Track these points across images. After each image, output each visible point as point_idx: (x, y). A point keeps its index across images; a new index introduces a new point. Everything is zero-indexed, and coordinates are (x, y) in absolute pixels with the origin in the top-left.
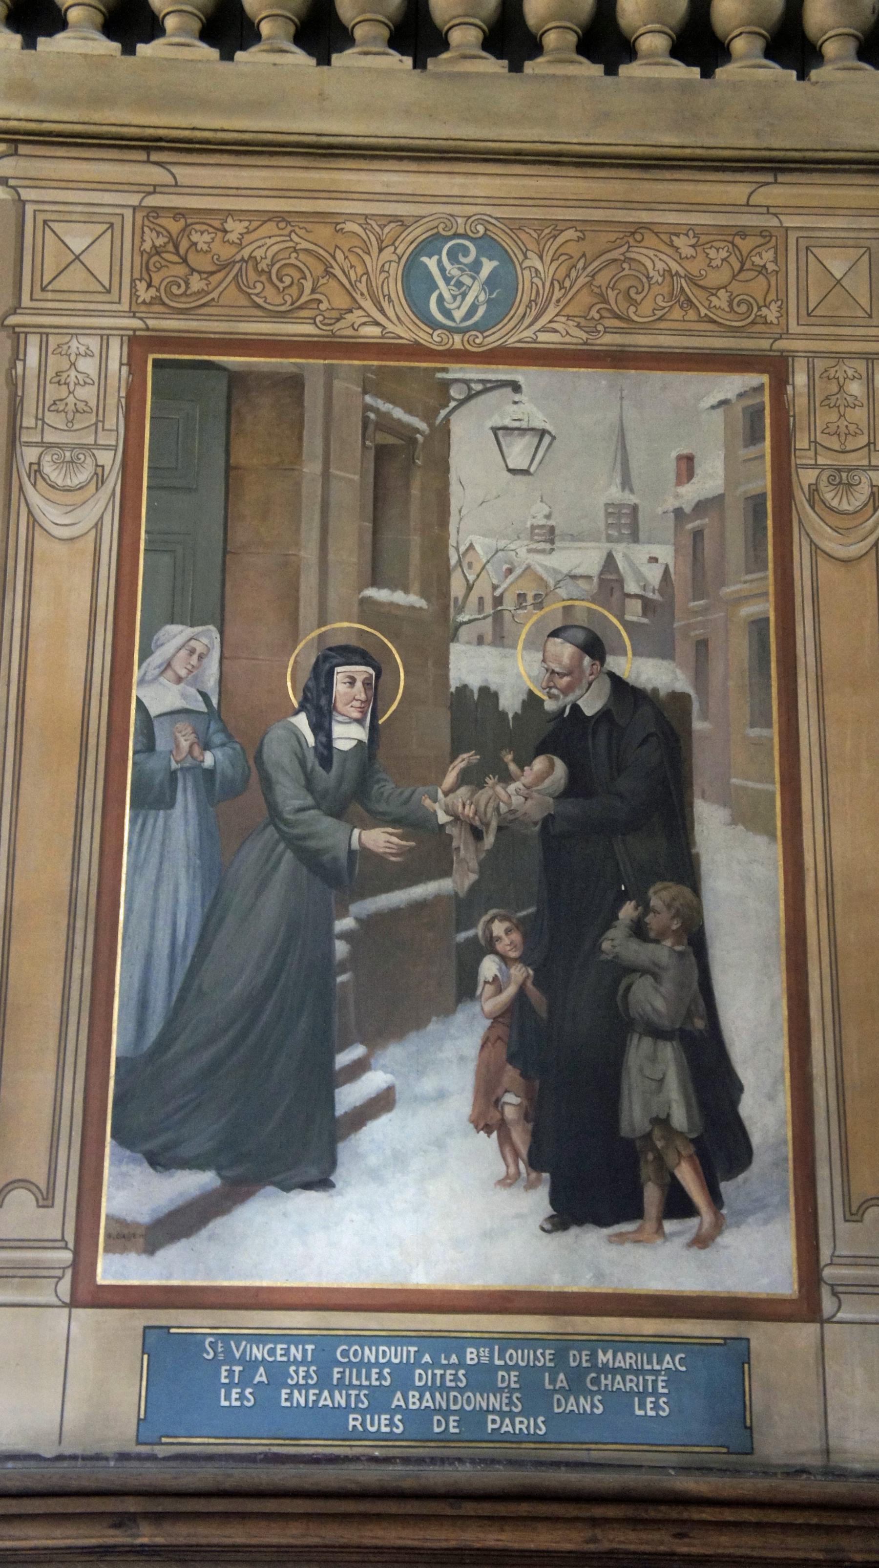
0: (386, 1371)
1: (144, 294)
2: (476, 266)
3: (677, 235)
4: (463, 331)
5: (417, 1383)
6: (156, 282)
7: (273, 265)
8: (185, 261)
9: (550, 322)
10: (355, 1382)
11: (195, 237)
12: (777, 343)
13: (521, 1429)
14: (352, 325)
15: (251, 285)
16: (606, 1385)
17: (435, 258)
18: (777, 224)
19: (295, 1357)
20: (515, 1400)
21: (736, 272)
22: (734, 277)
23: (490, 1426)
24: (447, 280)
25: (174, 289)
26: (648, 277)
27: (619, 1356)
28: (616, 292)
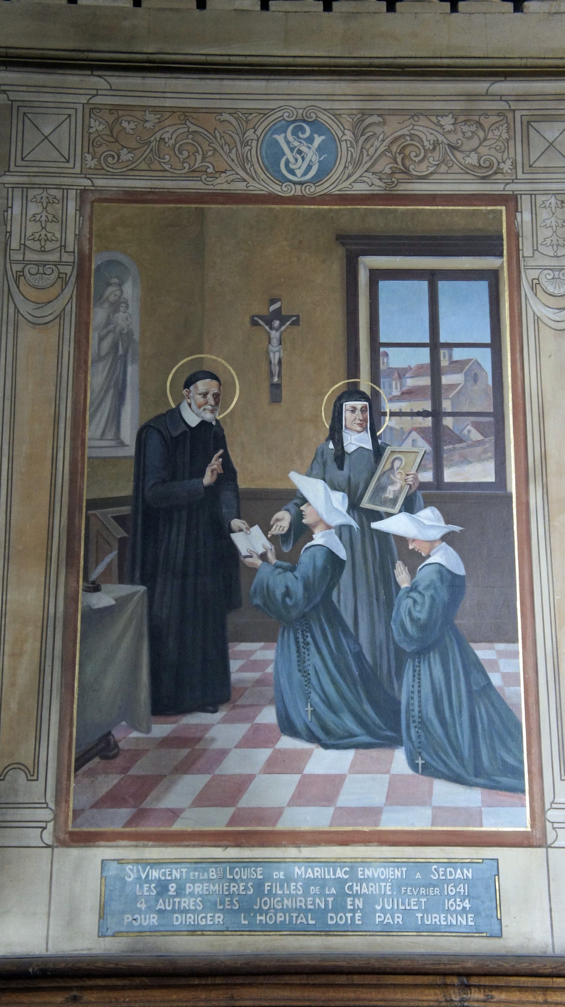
0: (250, 884)
1: (91, 163)
2: (310, 140)
3: (442, 116)
4: (301, 183)
5: (312, 893)
6: (98, 155)
7: (176, 144)
8: (117, 141)
9: (361, 176)
10: (279, 892)
11: (125, 124)
12: (508, 186)
13: (219, 922)
14: (227, 181)
15: (161, 156)
16: (357, 891)
17: (283, 135)
18: (508, 108)
19: (175, 877)
20: (235, 902)
21: (482, 140)
22: (480, 144)
23: (378, 920)
24: (292, 150)
25: (110, 160)
26: (424, 147)
27: (310, 870)
28: (402, 155)
